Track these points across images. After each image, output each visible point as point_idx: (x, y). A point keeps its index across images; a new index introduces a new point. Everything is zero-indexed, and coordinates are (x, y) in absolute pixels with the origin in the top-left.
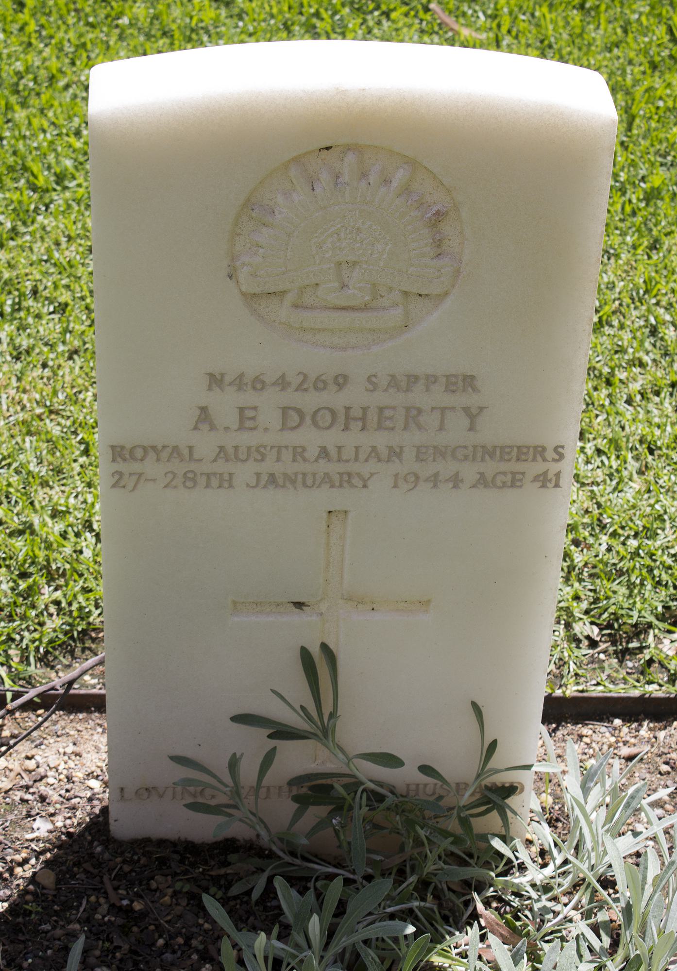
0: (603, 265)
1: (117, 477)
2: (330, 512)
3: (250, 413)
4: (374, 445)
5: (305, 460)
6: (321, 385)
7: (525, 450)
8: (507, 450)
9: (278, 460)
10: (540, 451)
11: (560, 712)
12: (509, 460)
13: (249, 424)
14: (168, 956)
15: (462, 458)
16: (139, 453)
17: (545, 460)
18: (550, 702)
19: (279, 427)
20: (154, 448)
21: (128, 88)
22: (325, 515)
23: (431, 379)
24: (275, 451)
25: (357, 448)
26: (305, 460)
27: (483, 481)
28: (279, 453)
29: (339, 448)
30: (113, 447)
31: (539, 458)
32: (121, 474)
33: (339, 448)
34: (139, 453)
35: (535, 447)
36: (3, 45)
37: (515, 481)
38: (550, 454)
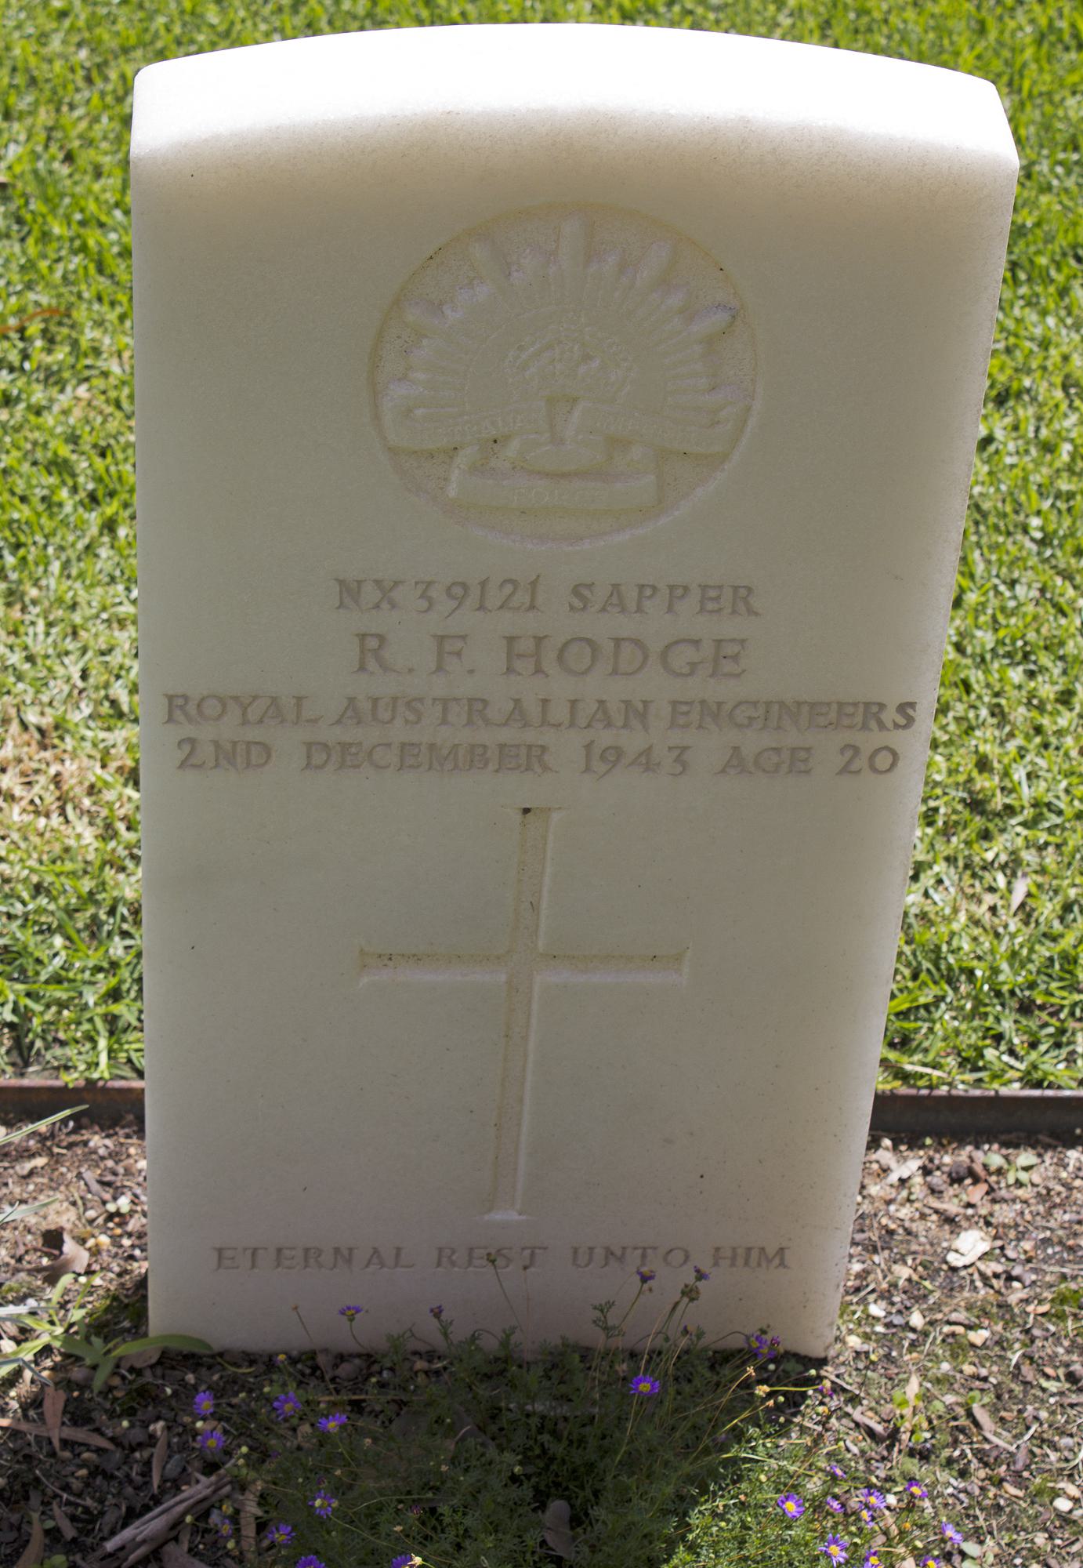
0: (986, 453)
1: (187, 748)
2: (526, 811)
3: (730, 649)
4: (604, 698)
5: (487, 722)
6: (458, 591)
7: (850, 710)
8: (685, 708)
9: (444, 721)
10: (872, 712)
11: (903, 1119)
12: (686, 726)
13: (728, 667)
14: (715, 1529)
15: (746, 722)
16: (212, 708)
17: (882, 726)
18: (882, 1102)
19: (433, 666)
20: (236, 698)
21: (194, 105)
22: (519, 817)
23: (677, 592)
24: (439, 708)
25: (574, 703)
26: (487, 722)
27: (736, 762)
28: (445, 710)
29: (299, 700)
30: (170, 698)
31: (873, 724)
32: (192, 741)
33: (299, 700)
34: (212, 708)
35: (867, 705)
36: (187, 5)
37: (798, 761)
38: (890, 715)
